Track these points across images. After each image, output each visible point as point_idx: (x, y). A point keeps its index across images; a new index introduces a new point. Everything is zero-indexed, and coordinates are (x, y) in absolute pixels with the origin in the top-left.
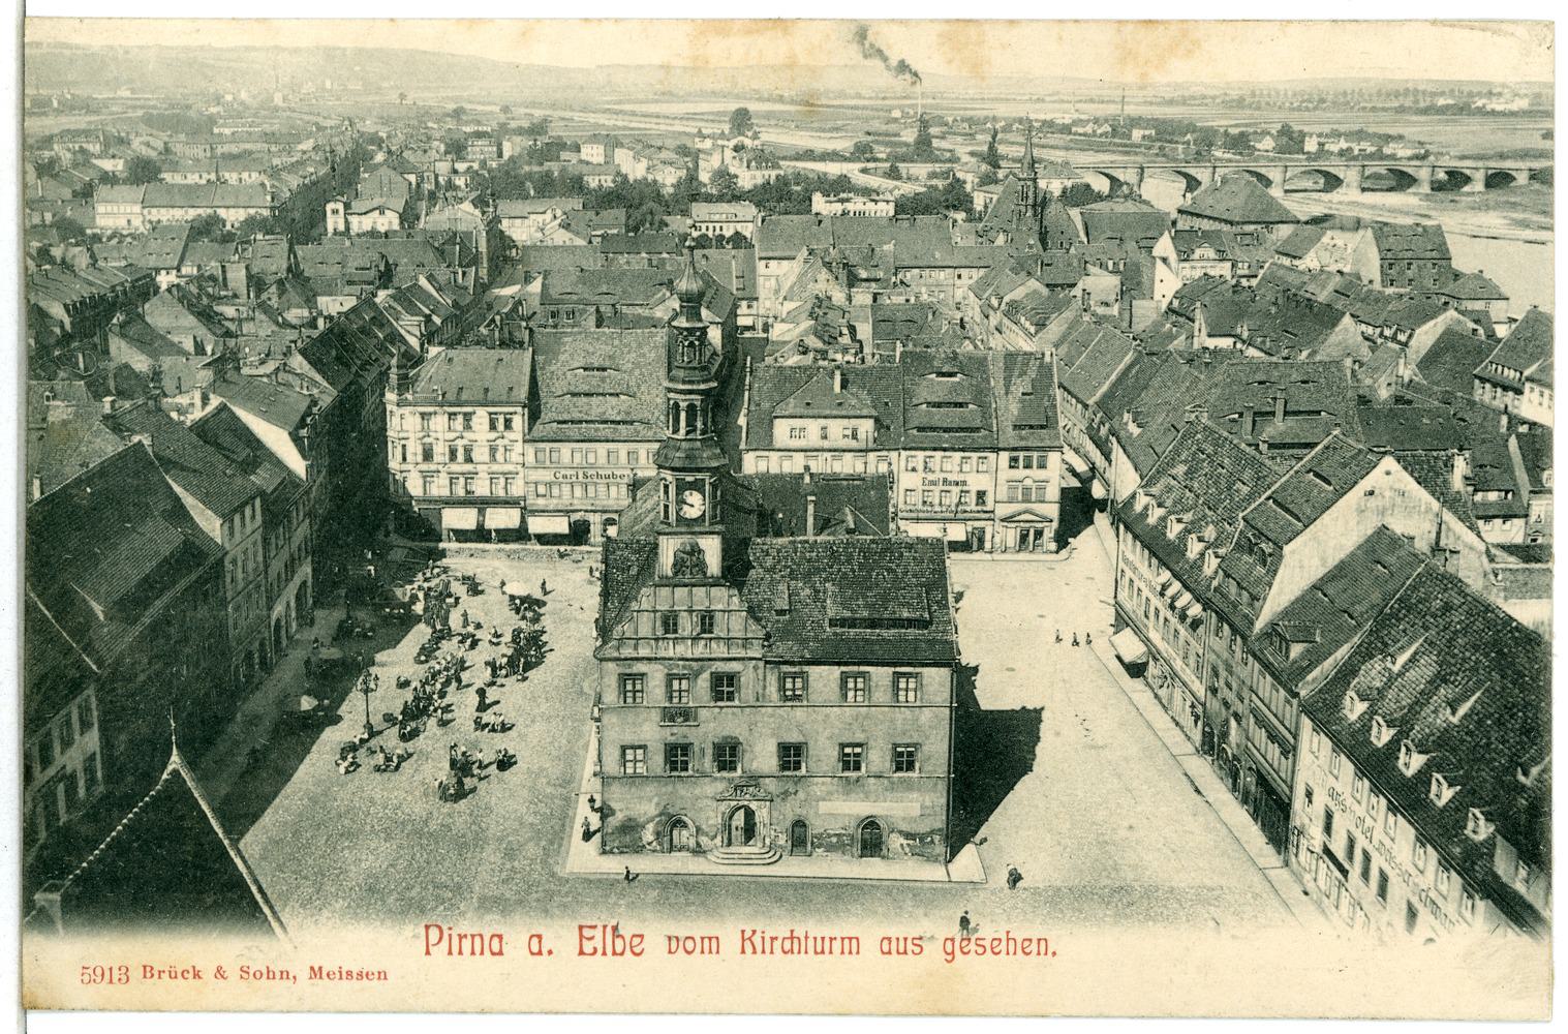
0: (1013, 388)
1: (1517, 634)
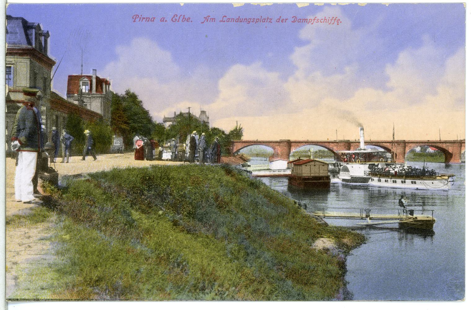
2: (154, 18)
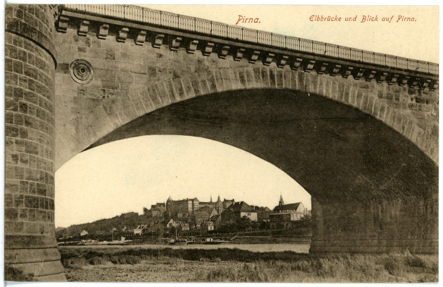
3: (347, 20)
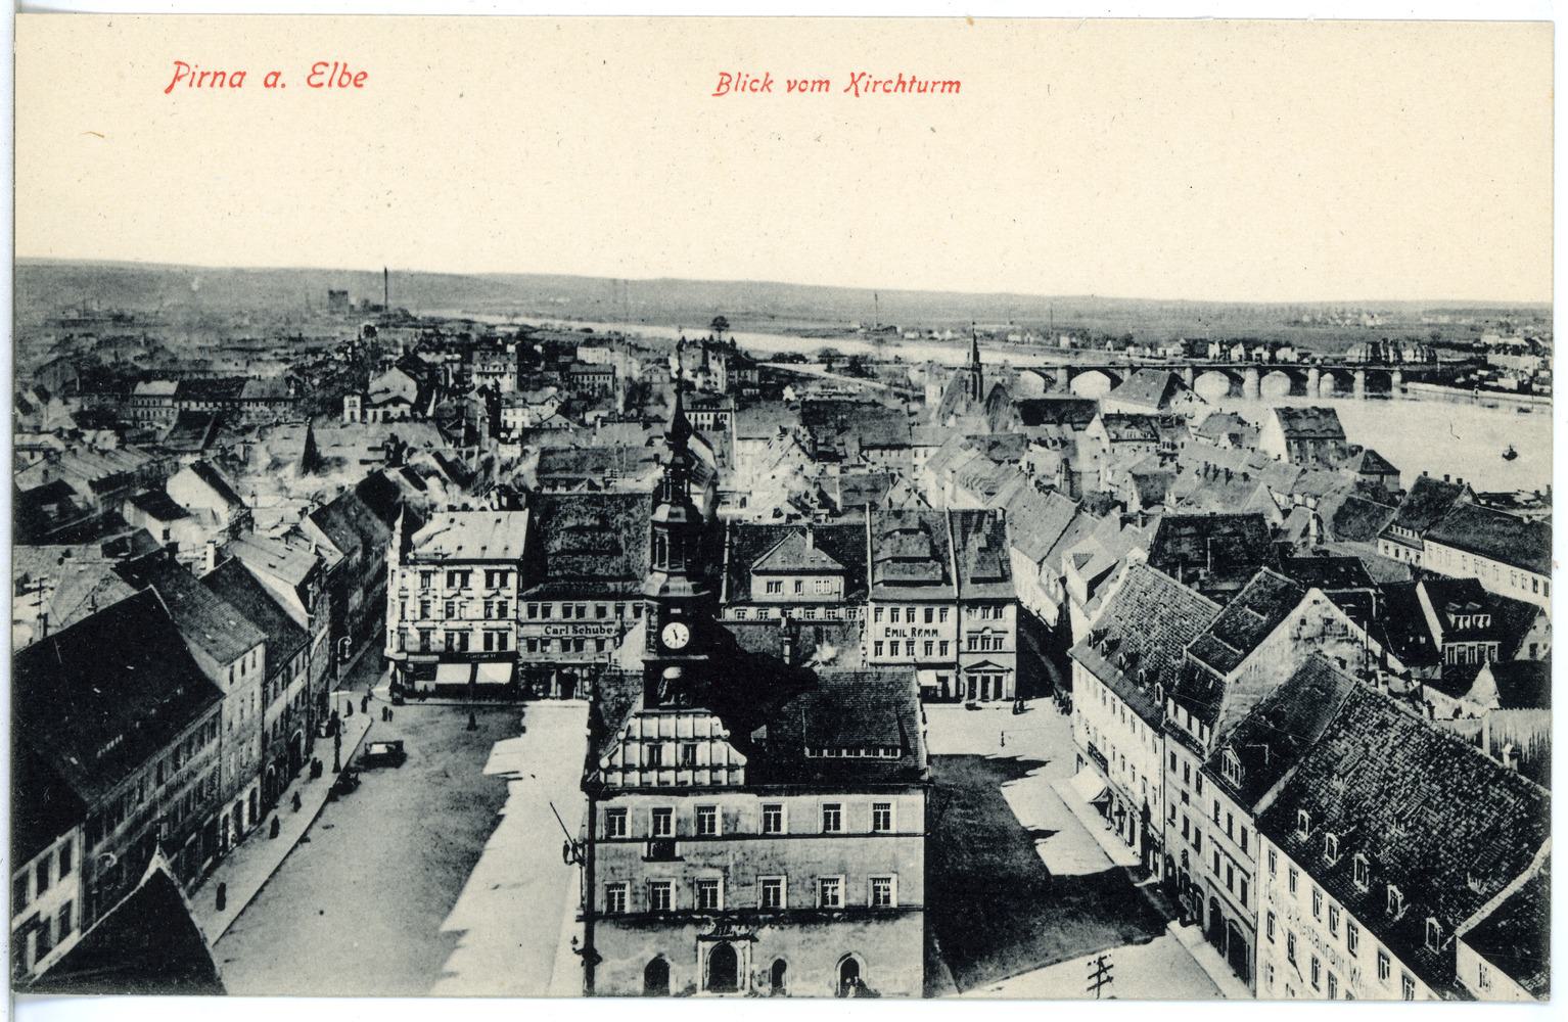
0: (969, 544)
1: (1451, 746)
2: (243, 74)
3: (925, 90)
